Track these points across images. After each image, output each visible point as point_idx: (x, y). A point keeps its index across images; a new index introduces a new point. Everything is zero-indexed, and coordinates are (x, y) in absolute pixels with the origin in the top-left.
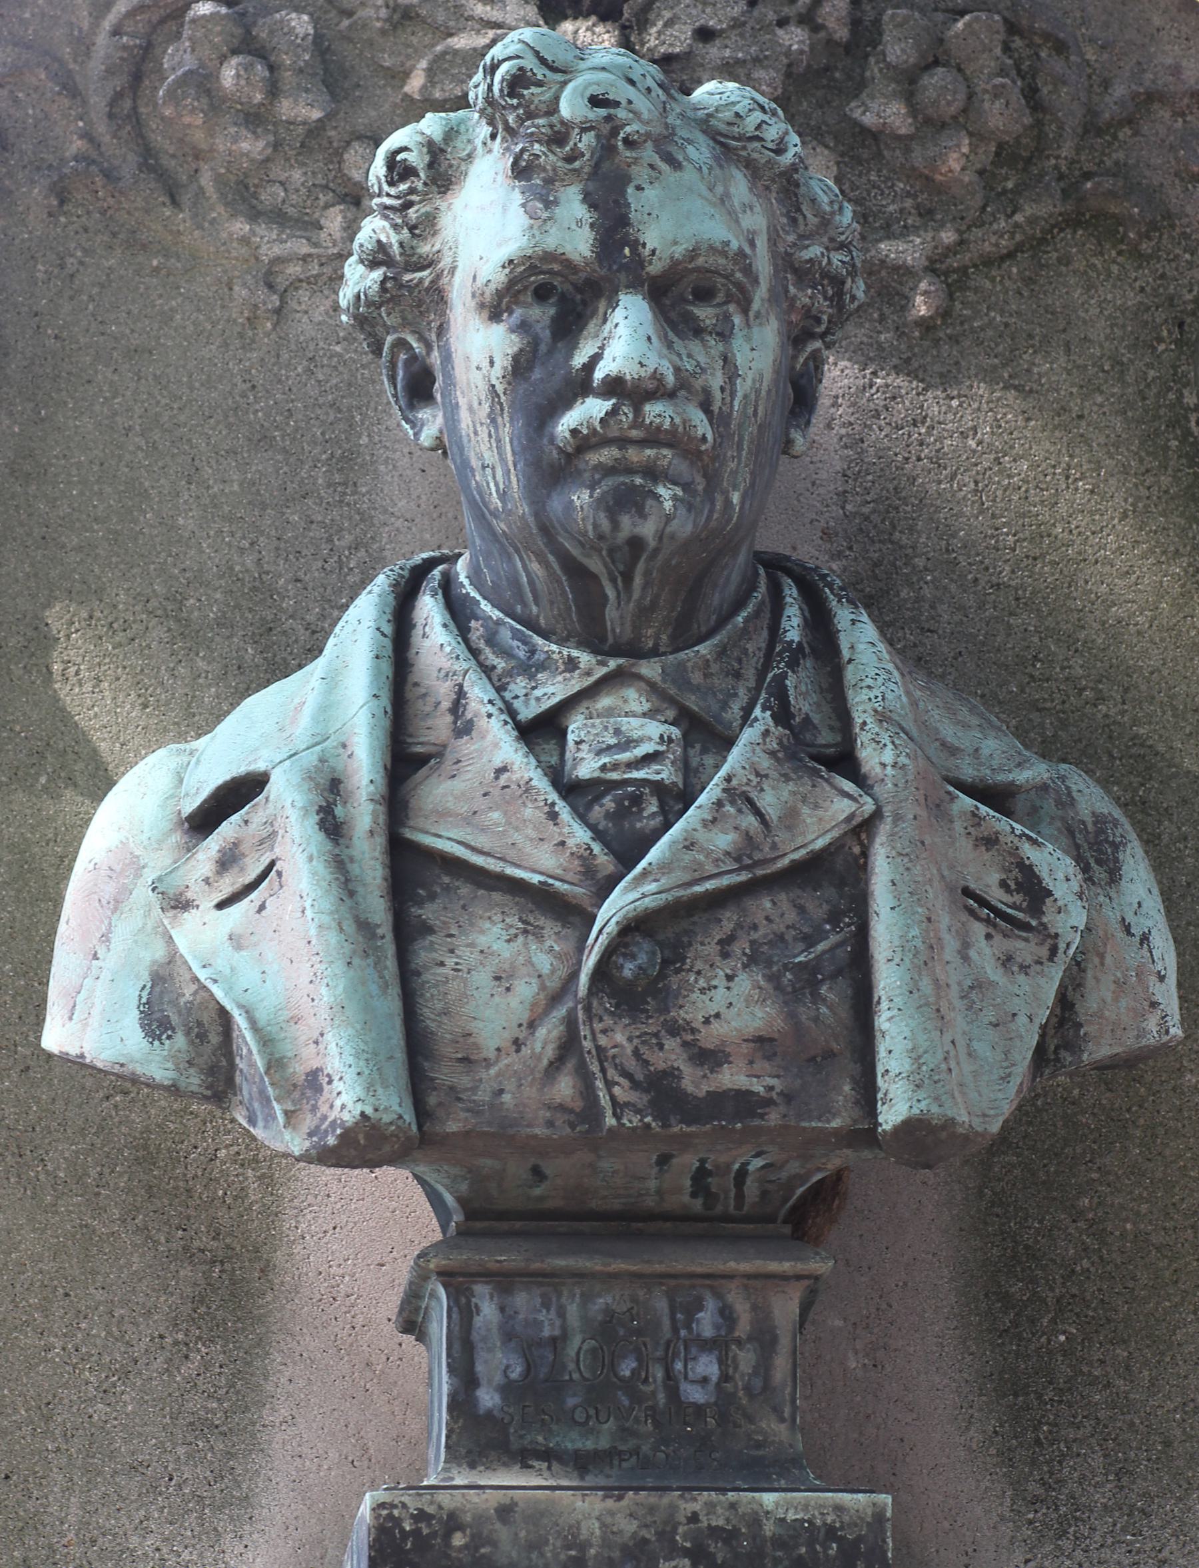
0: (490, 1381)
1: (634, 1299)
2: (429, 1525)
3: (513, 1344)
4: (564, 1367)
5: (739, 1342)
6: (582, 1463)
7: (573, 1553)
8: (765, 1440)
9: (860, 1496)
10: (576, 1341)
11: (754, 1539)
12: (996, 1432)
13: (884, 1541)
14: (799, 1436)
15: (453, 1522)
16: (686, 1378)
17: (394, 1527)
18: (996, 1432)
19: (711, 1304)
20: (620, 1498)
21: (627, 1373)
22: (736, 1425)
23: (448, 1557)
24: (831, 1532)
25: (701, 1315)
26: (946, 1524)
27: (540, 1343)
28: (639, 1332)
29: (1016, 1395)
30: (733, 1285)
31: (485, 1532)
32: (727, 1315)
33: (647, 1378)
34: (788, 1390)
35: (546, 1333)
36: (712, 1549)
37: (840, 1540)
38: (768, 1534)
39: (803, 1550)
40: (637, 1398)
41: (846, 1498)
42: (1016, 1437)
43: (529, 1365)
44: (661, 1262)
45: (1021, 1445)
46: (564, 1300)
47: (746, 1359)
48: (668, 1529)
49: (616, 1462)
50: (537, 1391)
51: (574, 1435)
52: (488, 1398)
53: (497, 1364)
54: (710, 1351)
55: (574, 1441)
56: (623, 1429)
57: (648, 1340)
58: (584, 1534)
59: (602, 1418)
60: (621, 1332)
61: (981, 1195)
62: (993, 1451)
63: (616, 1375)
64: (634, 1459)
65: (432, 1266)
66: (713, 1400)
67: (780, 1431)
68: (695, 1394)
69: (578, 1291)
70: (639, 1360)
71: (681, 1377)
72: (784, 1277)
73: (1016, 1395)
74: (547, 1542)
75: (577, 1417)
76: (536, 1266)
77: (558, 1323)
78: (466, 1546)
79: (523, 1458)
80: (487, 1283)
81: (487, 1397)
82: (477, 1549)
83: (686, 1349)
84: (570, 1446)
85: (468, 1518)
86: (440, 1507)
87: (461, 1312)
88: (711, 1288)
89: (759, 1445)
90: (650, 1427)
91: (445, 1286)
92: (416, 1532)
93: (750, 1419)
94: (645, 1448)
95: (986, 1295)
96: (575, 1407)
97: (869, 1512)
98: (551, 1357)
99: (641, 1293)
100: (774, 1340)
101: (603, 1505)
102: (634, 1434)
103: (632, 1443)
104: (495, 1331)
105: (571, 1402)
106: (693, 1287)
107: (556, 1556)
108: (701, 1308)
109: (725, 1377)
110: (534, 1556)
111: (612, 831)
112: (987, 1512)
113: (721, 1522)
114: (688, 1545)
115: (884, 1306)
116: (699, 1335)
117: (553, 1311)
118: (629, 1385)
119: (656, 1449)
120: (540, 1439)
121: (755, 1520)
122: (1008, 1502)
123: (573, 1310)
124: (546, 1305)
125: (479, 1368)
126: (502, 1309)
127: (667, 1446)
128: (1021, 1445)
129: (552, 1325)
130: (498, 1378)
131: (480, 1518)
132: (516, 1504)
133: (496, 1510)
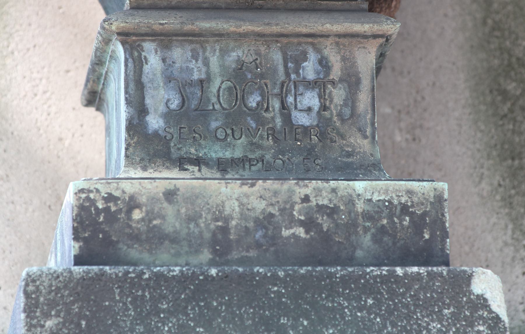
0: (156, 110)
1: (258, 53)
2: (116, 205)
3: (172, 85)
4: (209, 100)
5: (333, 83)
6: (223, 167)
7: (220, 224)
8: (354, 151)
9: (425, 183)
10: (217, 82)
11: (350, 213)
12: (500, 185)
13: (443, 215)
14: (378, 148)
15: (132, 203)
16: (296, 108)
17: (90, 206)
18: (500, 185)
19: (312, 56)
20: (253, 185)
21: (254, 105)
22: (332, 141)
23: (130, 227)
24: (405, 209)
25: (305, 64)
26: (467, 248)
27: (191, 84)
28: (262, 76)
29: (513, 159)
30: (328, 42)
31: (156, 210)
32: (324, 64)
33: (268, 108)
34: (369, 116)
35: (196, 76)
36: (319, 221)
37: (412, 215)
38: (360, 210)
39: (385, 222)
40: (261, 122)
41: (415, 185)
42: (514, 188)
43: (183, 99)
44: (277, 25)
45: (517, 193)
46: (207, 54)
47: (338, 94)
48: (288, 206)
49: (247, 166)
50: (191, 116)
51: (217, 147)
52: (155, 122)
53: (161, 99)
54: (313, 88)
55: (216, 152)
56: (252, 144)
57: (268, 81)
58: (227, 211)
59: (237, 135)
60: (249, 76)
61: (484, 23)
62: (498, 197)
63: (245, 106)
64: (260, 165)
65: (114, 28)
66: (315, 123)
67: (365, 145)
68: (302, 119)
69: (218, 47)
70: (262, 95)
71: (293, 107)
72: (365, 37)
73: (513, 159)
74: (201, 216)
75: (219, 136)
76: (188, 27)
77: (204, 69)
78: (143, 219)
79: (181, 163)
80: (153, 41)
81: (154, 122)
82: (150, 221)
83: (295, 88)
84: (214, 155)
85: (143, 199)
86: (124, 192)
87: (134, 62)
88: (313, 44)
89: (349, 155)
90: (271, 142)
91: (123, 43)
92: (107, 210)
93: (342, 137)
94: (268, 157)
95: (491, 91)
96: (217, 129)
97: (432, 194)
98: (199, 93)
99: (263, 49)
100: (358, 81)
101: (241, 190)
102: (259, 147)
103: (258, 154)
104: (159, 75)
105: (214, 125)
106: (299, 44)
107: (207, 226)
108: (305, 59)
109: (324, 108)
110: (192, 226)
111: (90, 233)
112: (495, 239)
113: (326, 202)
114: (302, 218)
115: (419, 99)
116: (304, 78)
117: (200, 62)
118: (255, 113)
119: (275, 158)
120: (193, 150)
121: (350, 201)
122: (509, 232)
123: (214, 61)
124: (195, 57)
125: (148, 101)
126: (164, 60)
127: (283, 155)
128: (517, 193)
129: (200, 71)
130: (162, 108)
131: (153, 200)
132: (178, 190)
133: (164, 194)
